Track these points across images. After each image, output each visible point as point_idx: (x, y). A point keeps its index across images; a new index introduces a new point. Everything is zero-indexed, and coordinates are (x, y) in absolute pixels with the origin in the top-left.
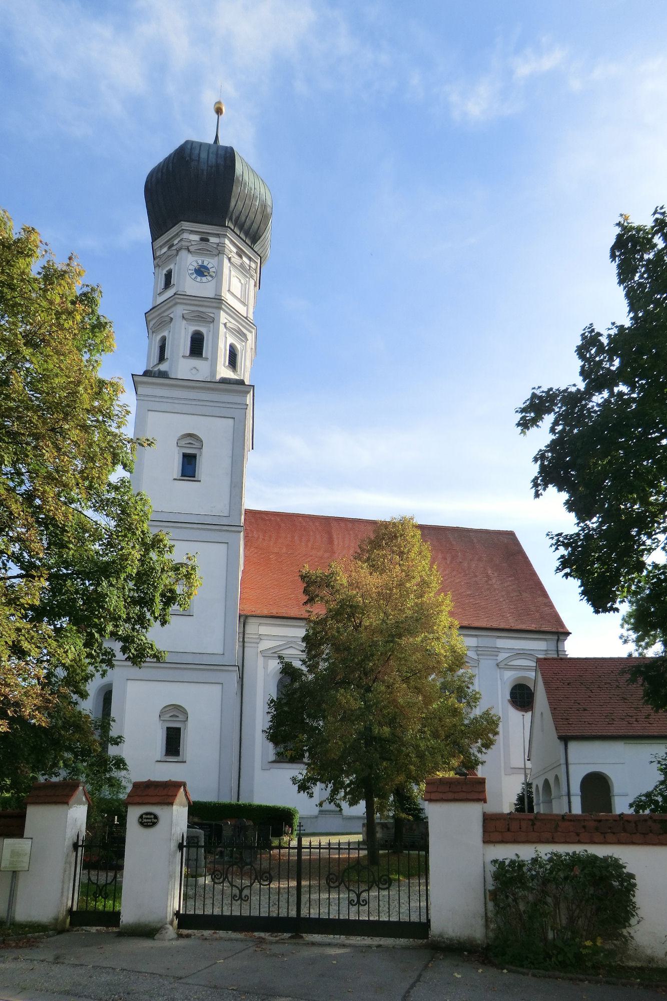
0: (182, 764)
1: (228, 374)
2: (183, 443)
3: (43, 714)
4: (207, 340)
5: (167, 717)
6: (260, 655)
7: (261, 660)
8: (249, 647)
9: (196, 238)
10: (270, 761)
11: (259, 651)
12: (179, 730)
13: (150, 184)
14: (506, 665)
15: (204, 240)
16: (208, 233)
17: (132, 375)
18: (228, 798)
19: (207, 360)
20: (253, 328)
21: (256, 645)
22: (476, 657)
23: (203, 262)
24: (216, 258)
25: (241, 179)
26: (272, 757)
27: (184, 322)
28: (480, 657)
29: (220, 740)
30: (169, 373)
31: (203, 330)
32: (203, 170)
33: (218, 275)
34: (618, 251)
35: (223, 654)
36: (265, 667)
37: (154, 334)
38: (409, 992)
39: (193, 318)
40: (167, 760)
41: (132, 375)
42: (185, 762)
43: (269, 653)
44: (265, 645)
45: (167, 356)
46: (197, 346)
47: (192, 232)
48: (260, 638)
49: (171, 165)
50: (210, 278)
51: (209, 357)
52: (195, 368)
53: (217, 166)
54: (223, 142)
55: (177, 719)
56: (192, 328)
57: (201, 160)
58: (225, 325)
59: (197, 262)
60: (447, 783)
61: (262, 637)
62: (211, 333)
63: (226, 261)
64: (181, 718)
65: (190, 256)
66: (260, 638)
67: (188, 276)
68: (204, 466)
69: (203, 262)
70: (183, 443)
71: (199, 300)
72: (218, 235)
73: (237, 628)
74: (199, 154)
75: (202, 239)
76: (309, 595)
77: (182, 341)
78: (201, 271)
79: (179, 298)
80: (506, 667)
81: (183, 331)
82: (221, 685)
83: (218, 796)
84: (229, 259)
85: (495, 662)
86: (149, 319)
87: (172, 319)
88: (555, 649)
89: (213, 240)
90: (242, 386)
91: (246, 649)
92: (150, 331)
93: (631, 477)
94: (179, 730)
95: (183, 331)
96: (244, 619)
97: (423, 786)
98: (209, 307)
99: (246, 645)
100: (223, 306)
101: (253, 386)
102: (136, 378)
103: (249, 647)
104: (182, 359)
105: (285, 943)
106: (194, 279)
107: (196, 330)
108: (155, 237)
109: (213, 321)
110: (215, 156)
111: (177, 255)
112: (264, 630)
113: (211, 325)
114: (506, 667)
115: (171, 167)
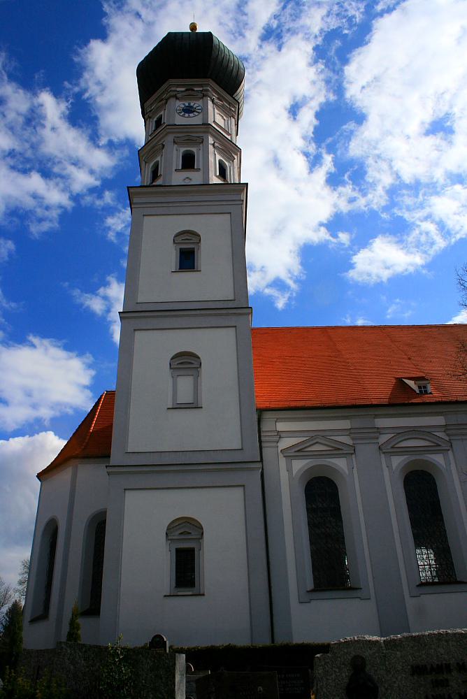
2: (179, 239)
5: (176, 535)
6: (281, 456)
7: (283, 462)
8: (267, 447)
10: (308, 590)
11: (279, 451)
14: (392, 447)
18: (263, 641)
21: (274, 444)
22: (447, 438)
23: (189, 104)
24: (201, 100)
26: (310, 586)
27: (176, 146)
28: (452, 438)
29: (249, 589)
31: (194, 150)
33: (204, 111)
35: (242, 449)
36: (289, 470)
38: (56, 177)
40: (179, 594)
41: (128, 187)
42: (203, 595)
43: (291, 453)
44: (286, 443)
46: (189, 162)
47: (179, 86)
48: (280, 435)
50: (197, 114)
51: (201, 168)
54: (254, 645)
55: (190, 537)
56: (182, 150)
58: (213, 145)
59: (184, 104)
61: (282, 435)
62: (201, 152)
63: (210, 103)
64: (194, 535)
65: (178, 101)
66: (280, 435)
68: (204, 257)
69: (189, 104)
70: (179, 239)
72: (201, 86)
73: (256, 417)
77: (174, 159)
78: (188, 110)
80: (395, 450)
81: (175, 152)
82: (241, 489)
83: (252, 641)
84: (213, 101)
85: (376, 447)
86: (141, 155)
87: (164, 146)
90: (229, 96)
91: (263, 450)
95: (175, 152)
96: (261, 411)
99: (263, 445)
100: (210, 130)
102: (131, 190)
103: (267, 447)
107: (187, 150)
109: (202, 142)
111: (166, 103)
112: (281, 426)
114: (395, 450)
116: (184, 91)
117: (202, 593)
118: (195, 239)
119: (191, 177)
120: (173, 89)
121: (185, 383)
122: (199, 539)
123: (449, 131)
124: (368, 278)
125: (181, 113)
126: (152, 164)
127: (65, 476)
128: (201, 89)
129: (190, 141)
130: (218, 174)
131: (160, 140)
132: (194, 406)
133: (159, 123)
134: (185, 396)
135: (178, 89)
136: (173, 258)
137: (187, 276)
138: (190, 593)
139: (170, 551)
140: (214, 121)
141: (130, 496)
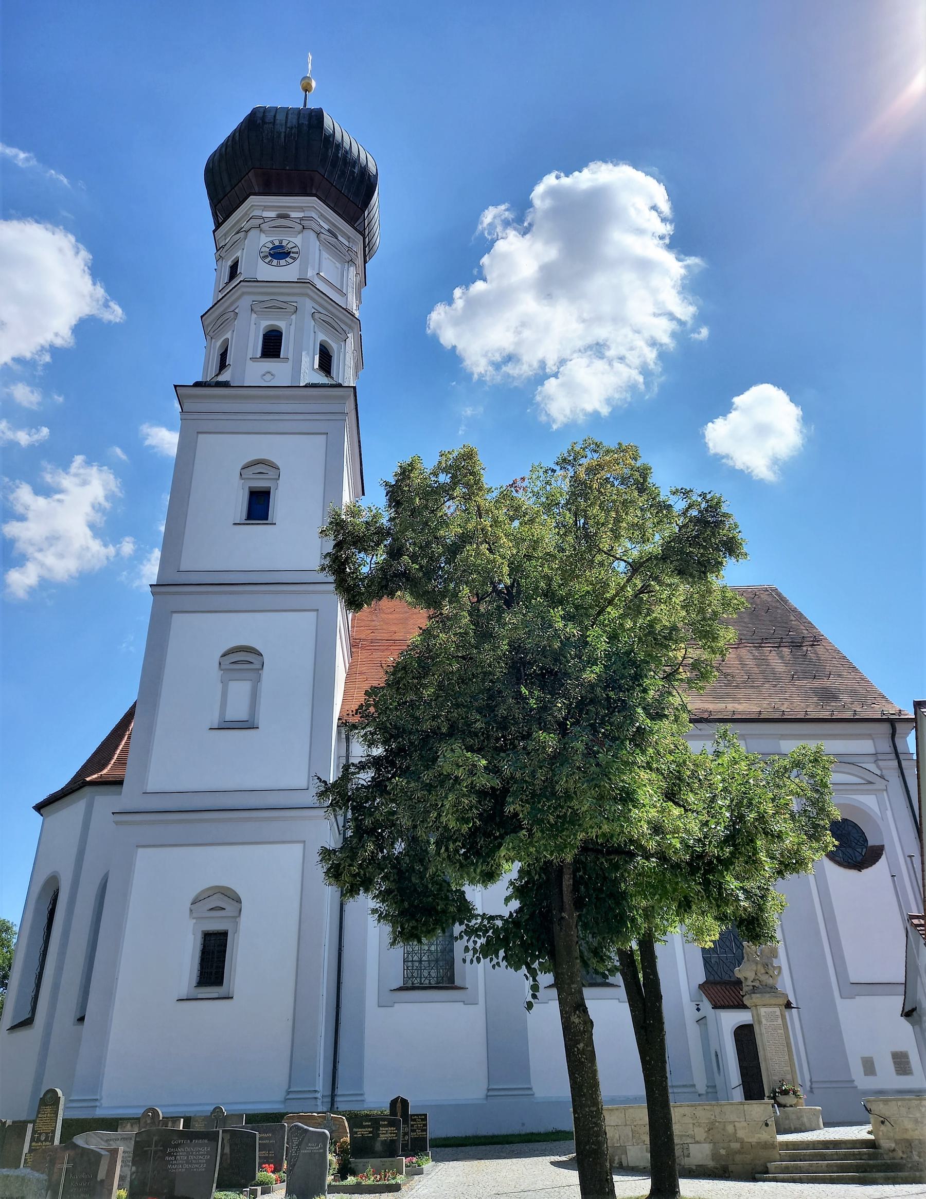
1: (321, 379)
12: (224, 934)
13: (211, 165)
16: (288, 207)
17: (175, 386)
20: (356, 323)
23: (281, 242)
24: (300, 236)
25: (331, 139)
27: (254, 316)
30: (230, 383)
31: (282, 325)
32: (279, 133)
37: (213, 340)
41: (175, 386)
45: (230, 361)
47: (266, 208)
49: (237, 134)
51: (290, 356)
53: (299, 126)
56: (265, 324)
57: (278, 122)
60: (638, 1172)
62: (293, 328)
64: (230, 909)
65: (263, 235)
68: (279, 506)
70: (248, 472)
74: (275, 116)
76: (441, 912)
78: (279, 254)
81: (253, 327)
86: (206, 323)
88: (891, 750)
92: (208, 337)
93: (650, 1022)
94: (224, 934)
95: (253, 327)
97: (829, 849)
101: (379, 1006)
104: (249, 363)
105: (891, 1100)
106: (269, 263)
108: (218, 225)
110: (296, 117)
113: (293, 317)
115: (238, 137)
116: (273, 219)
117: (230, 996)
118: (272, 473)
119: (273, 372)
120: (256, 213)
121: (240, 690)
122: (235, 917)
123: (524, 480)
124: (567, 480)
125: (266, 257)
126: (219, 343)
127: (74, 810)
128: (301, 215)
129: (278, 308)
130: (316, 366)
131: (232, 304)
132: (249, 725)
133: (234, 271)
134: (238, 710)
135: (266, 214)
136: (239, 504)
137: (257, 530)
138: (216, 995)
139: (194, 934)
140: (243, 294)
141: (142, 854)
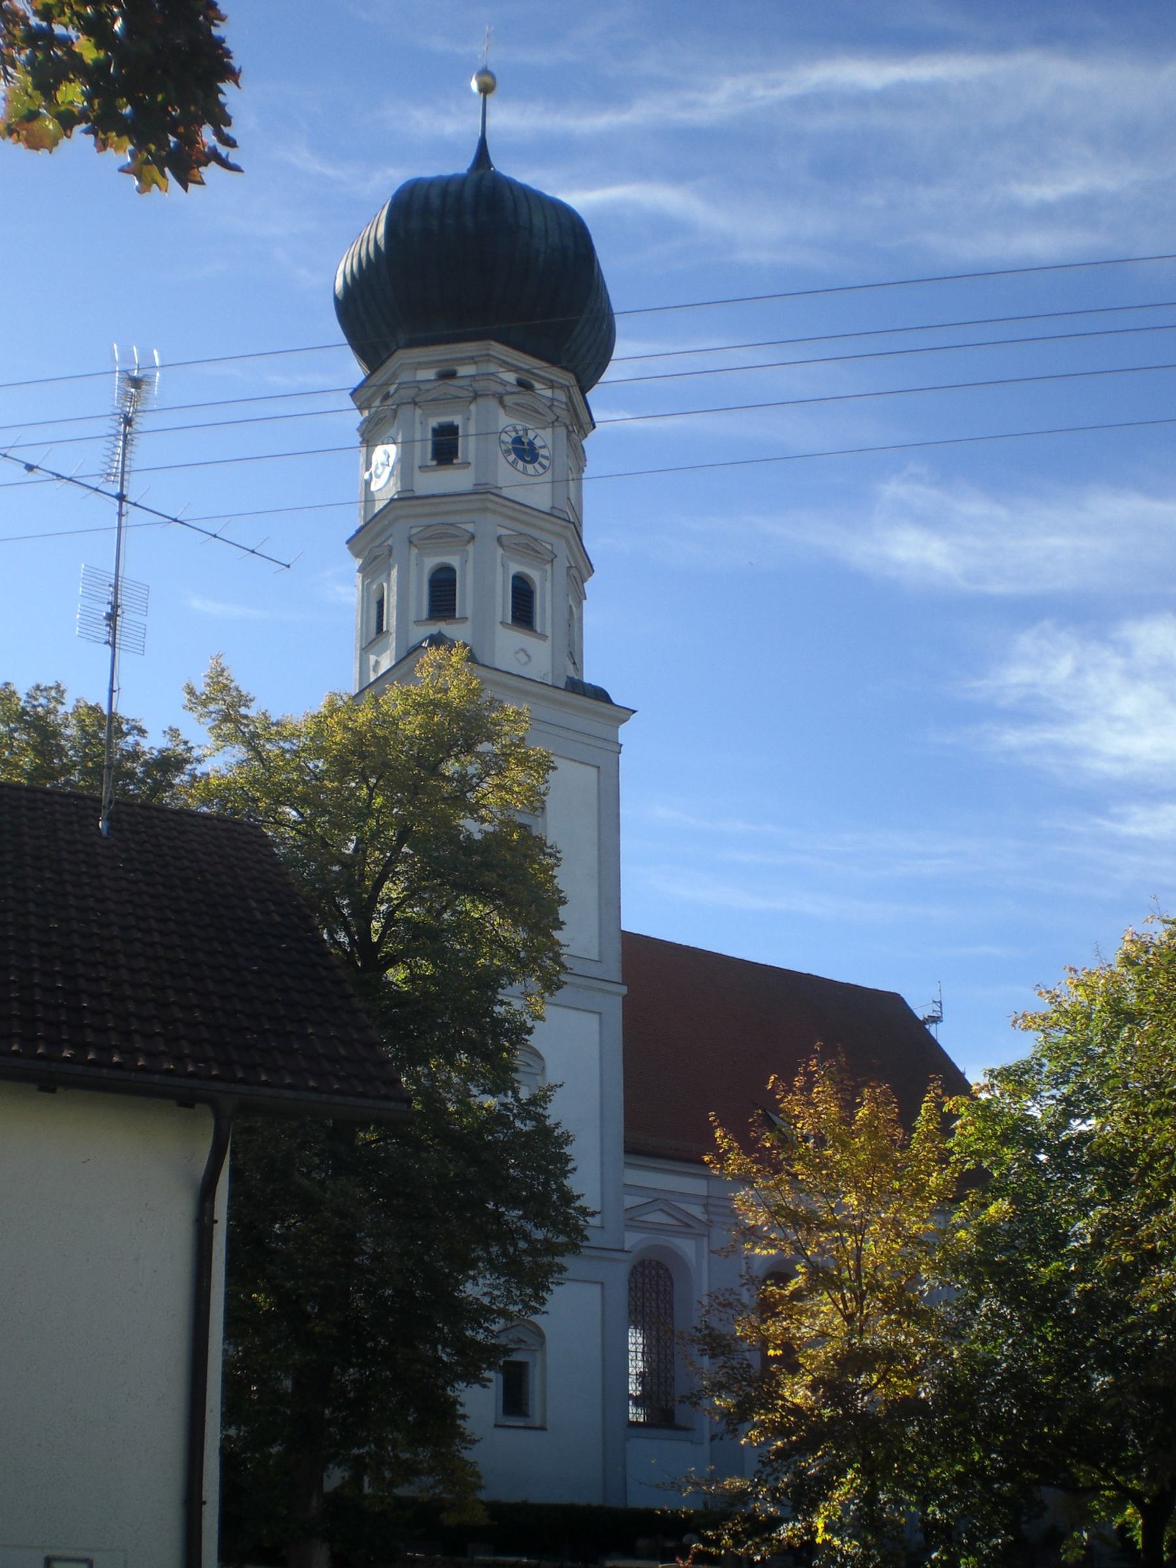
0: (539, 1432)
3: (535, 1113)
4: (543, 595)
9: (511, 377)
15: (524, 385)
19: (544, 640)
24: (549, 430)
34: (1126, 1450)
39: (515, 547)
40: (508, 1423)
47: (504, 364)
52: (523, 650)
56: (431, 562)
65: (501, 412)
67: (501, 455)
69: (526, 430)
71: (515, 510)
75: (521, 383)
79: (492, 501)
89: (464, 370)
98: (542, 529)
106: (513, 464)
